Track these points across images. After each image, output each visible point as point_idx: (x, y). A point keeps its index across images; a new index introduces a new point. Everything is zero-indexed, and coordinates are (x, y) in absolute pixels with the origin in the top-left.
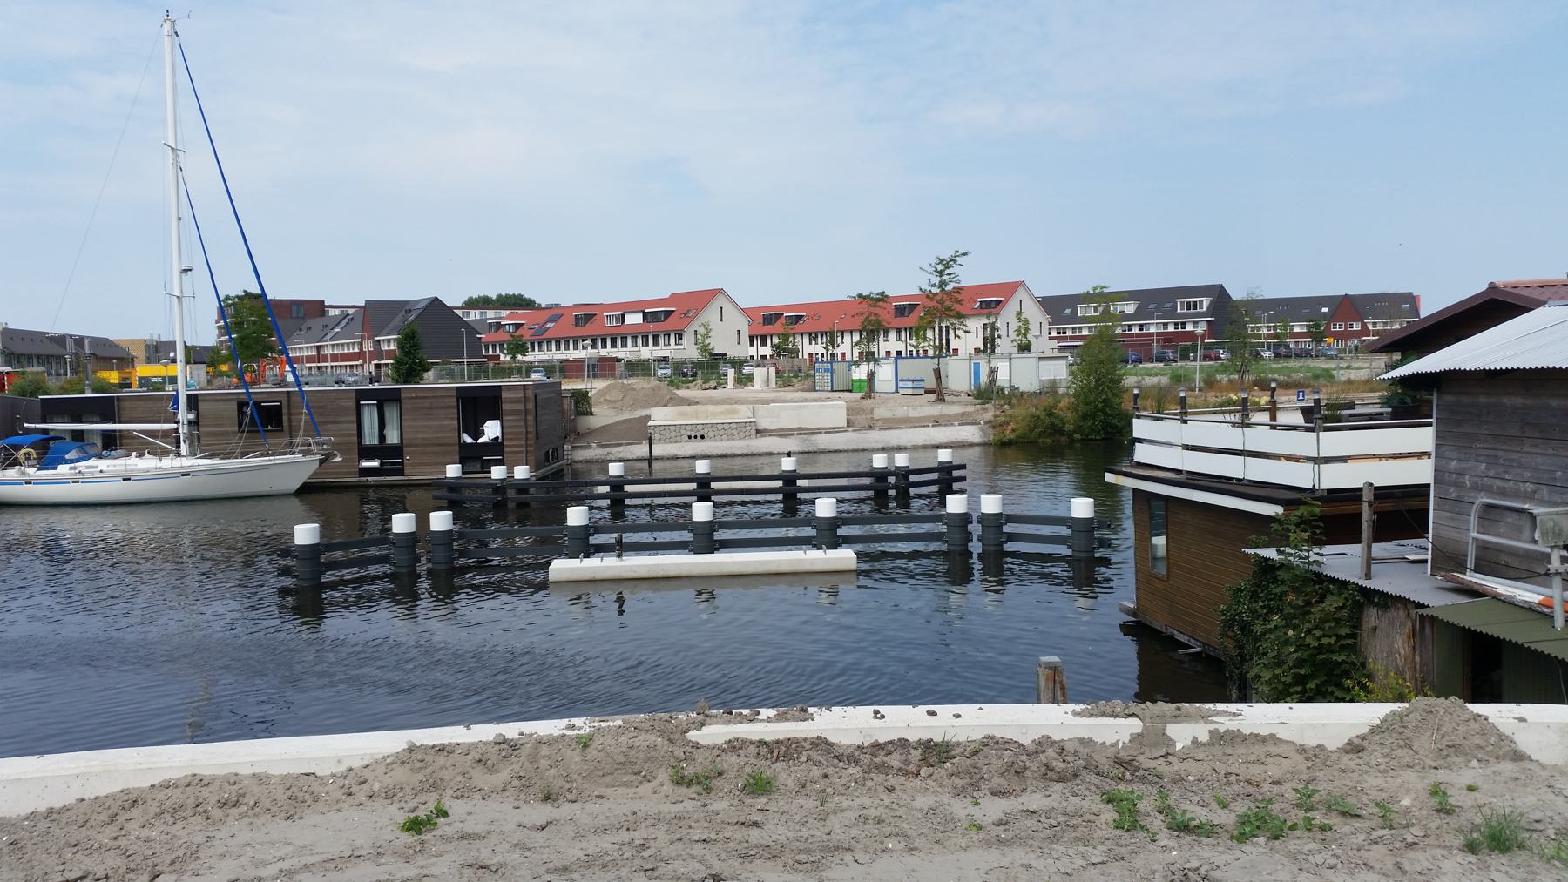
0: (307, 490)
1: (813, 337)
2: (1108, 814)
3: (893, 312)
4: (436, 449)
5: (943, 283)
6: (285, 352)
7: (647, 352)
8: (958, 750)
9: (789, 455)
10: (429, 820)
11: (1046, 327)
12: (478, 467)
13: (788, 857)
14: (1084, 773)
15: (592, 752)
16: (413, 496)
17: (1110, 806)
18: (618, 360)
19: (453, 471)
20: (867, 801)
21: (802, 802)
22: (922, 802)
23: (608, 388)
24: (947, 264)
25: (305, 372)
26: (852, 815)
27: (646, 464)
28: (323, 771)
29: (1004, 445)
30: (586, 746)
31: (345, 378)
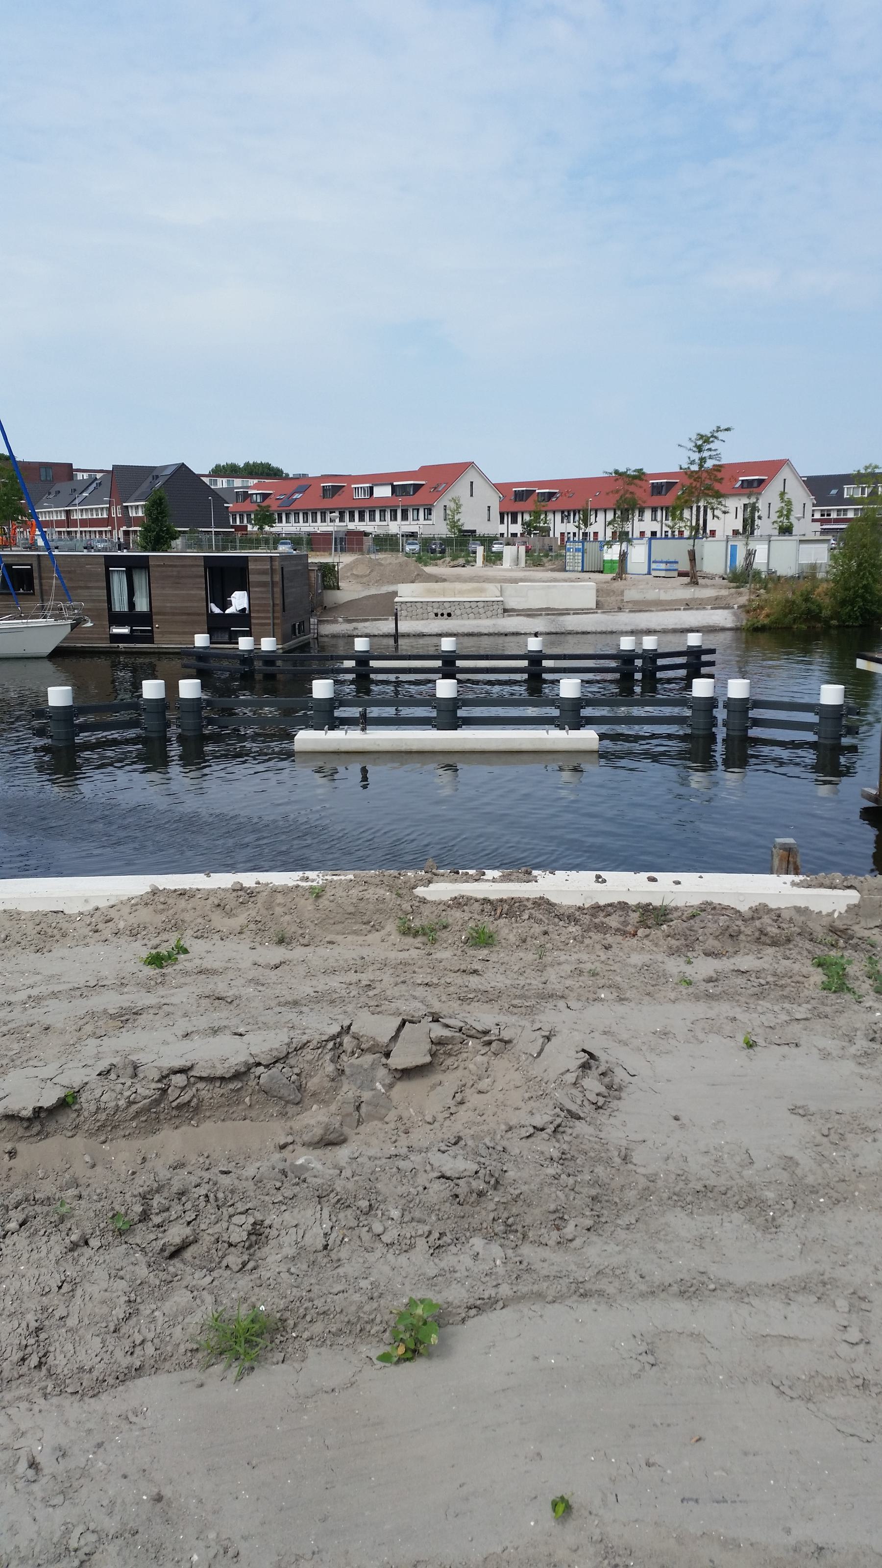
0: (59, 654)
1: (566, 515)
2: (818, 976)
3: (649, 490)
4: (184, 617)
5: (703, 460)
6: (35, 516)
7: (395, 527)
8: (676, 914)
9: (536, 635)
10: (170, 957)
11: (809, 508)
12: (226, 638)
13: (504, 1002)
14: (798, 939)
15: (324, 902)
16: (163, 665)
17: (820, 970)
18: (366, 534)
19: (201, 640)
20: (584, 957)
21: (522, 955)
22: (637, 959)
23: (354, 562)
24: (704, 441)
25: (55, 537)
26: (568, 968)
27: (391, 641)
28: (72, 909)
29: (756, 630)
30: (318, 896)
31: (94, 544)
